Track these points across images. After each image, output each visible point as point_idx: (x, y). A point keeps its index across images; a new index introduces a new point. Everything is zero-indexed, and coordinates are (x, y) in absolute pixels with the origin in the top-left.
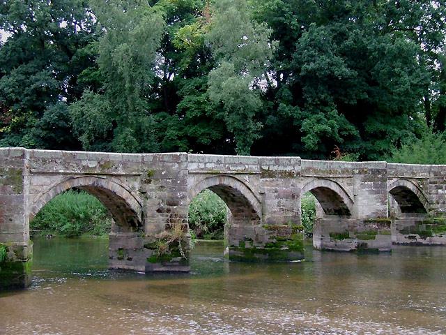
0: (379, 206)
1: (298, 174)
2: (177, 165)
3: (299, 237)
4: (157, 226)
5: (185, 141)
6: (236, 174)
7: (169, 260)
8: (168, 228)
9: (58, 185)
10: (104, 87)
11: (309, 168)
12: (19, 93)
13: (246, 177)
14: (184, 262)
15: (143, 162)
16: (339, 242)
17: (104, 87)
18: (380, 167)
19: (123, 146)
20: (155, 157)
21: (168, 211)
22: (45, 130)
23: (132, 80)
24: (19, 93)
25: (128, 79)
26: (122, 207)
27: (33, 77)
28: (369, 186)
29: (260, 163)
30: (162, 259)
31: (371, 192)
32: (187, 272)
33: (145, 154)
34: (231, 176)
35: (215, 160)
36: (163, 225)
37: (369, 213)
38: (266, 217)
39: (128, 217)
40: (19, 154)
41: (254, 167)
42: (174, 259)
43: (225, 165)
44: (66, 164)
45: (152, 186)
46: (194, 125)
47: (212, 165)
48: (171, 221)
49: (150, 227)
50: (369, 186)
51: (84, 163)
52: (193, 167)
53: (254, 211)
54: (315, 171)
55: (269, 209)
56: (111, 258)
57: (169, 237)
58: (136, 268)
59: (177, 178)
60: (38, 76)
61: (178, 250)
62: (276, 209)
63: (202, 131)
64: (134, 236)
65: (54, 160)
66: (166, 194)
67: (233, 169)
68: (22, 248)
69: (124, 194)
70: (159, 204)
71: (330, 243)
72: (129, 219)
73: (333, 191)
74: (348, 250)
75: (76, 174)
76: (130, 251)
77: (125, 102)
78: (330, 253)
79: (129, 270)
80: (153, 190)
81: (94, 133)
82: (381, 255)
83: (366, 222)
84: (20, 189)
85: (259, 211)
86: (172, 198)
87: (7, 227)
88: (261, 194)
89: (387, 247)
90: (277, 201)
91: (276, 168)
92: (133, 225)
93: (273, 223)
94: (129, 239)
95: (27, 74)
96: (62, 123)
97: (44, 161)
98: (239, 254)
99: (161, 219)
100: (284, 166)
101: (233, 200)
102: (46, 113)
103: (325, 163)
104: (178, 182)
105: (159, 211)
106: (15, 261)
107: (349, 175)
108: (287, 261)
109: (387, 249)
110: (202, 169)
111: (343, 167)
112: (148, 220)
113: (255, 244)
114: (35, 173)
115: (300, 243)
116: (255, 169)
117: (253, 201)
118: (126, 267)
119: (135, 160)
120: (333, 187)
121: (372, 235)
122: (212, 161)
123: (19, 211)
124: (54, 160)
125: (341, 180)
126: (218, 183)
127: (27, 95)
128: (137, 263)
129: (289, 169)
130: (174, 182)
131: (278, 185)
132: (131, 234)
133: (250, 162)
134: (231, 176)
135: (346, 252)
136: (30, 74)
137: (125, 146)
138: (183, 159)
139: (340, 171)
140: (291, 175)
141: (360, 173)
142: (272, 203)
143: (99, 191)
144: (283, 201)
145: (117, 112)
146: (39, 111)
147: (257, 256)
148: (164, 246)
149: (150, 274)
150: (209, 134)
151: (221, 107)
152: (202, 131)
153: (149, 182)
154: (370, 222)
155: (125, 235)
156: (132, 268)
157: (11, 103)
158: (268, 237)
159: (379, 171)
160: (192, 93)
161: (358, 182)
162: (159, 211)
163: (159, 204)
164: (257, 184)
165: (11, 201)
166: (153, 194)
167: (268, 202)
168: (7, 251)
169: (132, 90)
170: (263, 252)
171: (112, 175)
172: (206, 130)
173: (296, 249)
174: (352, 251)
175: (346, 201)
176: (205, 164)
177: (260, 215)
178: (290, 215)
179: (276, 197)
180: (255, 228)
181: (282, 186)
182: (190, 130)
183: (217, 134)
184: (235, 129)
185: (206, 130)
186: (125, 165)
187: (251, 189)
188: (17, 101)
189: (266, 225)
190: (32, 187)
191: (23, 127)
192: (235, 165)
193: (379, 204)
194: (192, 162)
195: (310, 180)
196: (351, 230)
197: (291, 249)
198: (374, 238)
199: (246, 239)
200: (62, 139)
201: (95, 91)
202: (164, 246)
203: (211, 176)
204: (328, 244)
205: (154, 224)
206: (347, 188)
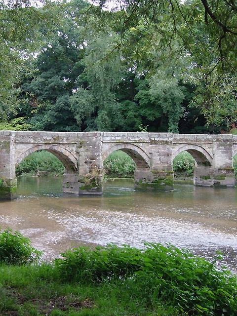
0: (228, 161)
1: (171, 142)
2: (95, 138)
3: (171, 178)
4: (85, 170)
5: (140, 118)
6: (134, 142)
7: (90, 189)
8: (90, 172)
9: (30, 149)
10: (90, 86)
11: (182, 139)
12: (42, 90)
13: (141, 144)
14: (99, 190)
15: (78, 137)
16: (205, 181)
17: (90, 86)
18: (228, 138)
19: (100, 122)
20: (84, 134)
21: (91, 162)
22: (57, 112)
23: (105, 81)
24: (42, 90)
25: (102, 81)
26: (67, 161)
27: (50, 80)
28: (222, 149)
29: (150, 136)
30: (87, 188)
31: (223, 152)
32: (100, 195)
33: (78, 133)
34: (130, 144)
35: (122, 135)
36: (88, 170)
37: (222, 165)
38: (153, 167)
39: (71, 166)
40: (8, 134)
41: (146, 138)
42: (94, 188)
43: (127, 138)
44: (34, 138)
45: (82, 149)
46: (145, 108)
47: (120, 138)
48: (92, 168)
49: (81, 171)
50: (222, 149)
51: (44, 138)
52: (108, 139)
53: (146, 163)
54: (186, 140)
55: (154, 162)
56: (63, 187)
57: (90, 177)
58: (75, 193)
59: (95, 145)
60: (52, 79)
61: (95, 184)
62: (159, 162)
63: (149, 112)
64: (74, 176)
65: (28, 136)
66: (89, 153)
67: (132, 140)
68: (10, 180)
69: (67, 154)
70: (86, 159)
71: (200, 182)
72: (72, 167)
73: (200, 152)
74: (209, 186)
75: (41, 143)
76: (72, 184)
77: (101, 95)
78: (200, 188)
79: (71, 193)
80: (82, 151)
81: (84, 114)
82: (227, 190)
83: (220, 169)
84: (8, 151)
85: (149, 163)
86: (93, 156)
87: (3, 170)
88: (150, 153)
89: (232, 185)
90: (159, 157)
91: (158, 139)
92: (74, 170)
93: (157, 170)
94: (70, 177)
95: (47, 78)
96: (66, 108)
97: (23, 137)
98: (139, 186)
99: (87, 167)
100: (163, 138)
101: (135, 157)
102: (57, 101)
103: (193, 136)
104: (96, 148)
105: (86, 163)
106: (6, 186)
107: (210, 142)
108: (163, 190)
109: (231, 186)
110: (114, 140)
111: (205, 138)
112: (80, 167)
113: (147, 181)
114: (18, 143)
115: (171, 181)
116: (147, 139)
117: (145, 157)
118: (70, 192)
119: (73, 135)
120: (199, 149)
121: (223, 177)
122: (119, 135)
123: (8, 162)
124: (28, 136)
125: (204, 145)
126: (123, 148)
127: (46, 91)
128: (75, 190)
129: (166, 139)
130: (94, 147)
131: (159, 149)
132: (73, 174)
133: (144, 135)
134: (130, 144)
135: (209, 187)
136: (48, 78)
137: (102, 122)
138: (98, 135)
139: (203, 140)
140: (167, 143)
141: (216, 141)
142: (156, 158)
143: (55, 152)
144: (163, 157)
145: (96, 101)
146: (53, 100)
147: (148, 188)
148: (88, 181)
149: (81, 195)
150: (154, 114)
151: (158, 98)
152: (149, 112)
153: (81, 147)
154: (222, 169)
155: (70, 175)
156: (73, 192)
157: (37, 95)
158: (154, 177)
159: (227, 140)
160: (143, 88)
161: (215, 146)
162: (86, 163)
163: (86, 159)
164: (148, 148)
165: (4, 157)
166: (83, 154)
167: (154, 158)
168: (3, 181)
169: (105, 87)
170: (152, 186)
171: (60, 144)
172: (152, 112)
173: (169, 184)
174: (211, 186)
175: (208, 157)
176: (115, 137)
177: (149, 165)
178: (166, 165)
179: (159, 155)
180: (148, 172)
181: (162, 149)
182: (142, 112)
183: (159, 114)
184: (168, 111)
185: (152, 112)
186: (67, 139)
187: (144, 151)
188: (41, 94)
189: (153, 171)
190: (16, 150)
191: (45, 110)
192: (133, 137)
193: (227, 159)
194: (107, 136)
195: (182, 145)
196: (211, 174)
197: (166, 184)
198: (224, 179)
199: (143, 178)
200: (67, 117)
201: (85, 88)
202: (88, 181)
203: (119, 143)
204: (199, 182)
205: (83, 169)
206: (208, 150)
